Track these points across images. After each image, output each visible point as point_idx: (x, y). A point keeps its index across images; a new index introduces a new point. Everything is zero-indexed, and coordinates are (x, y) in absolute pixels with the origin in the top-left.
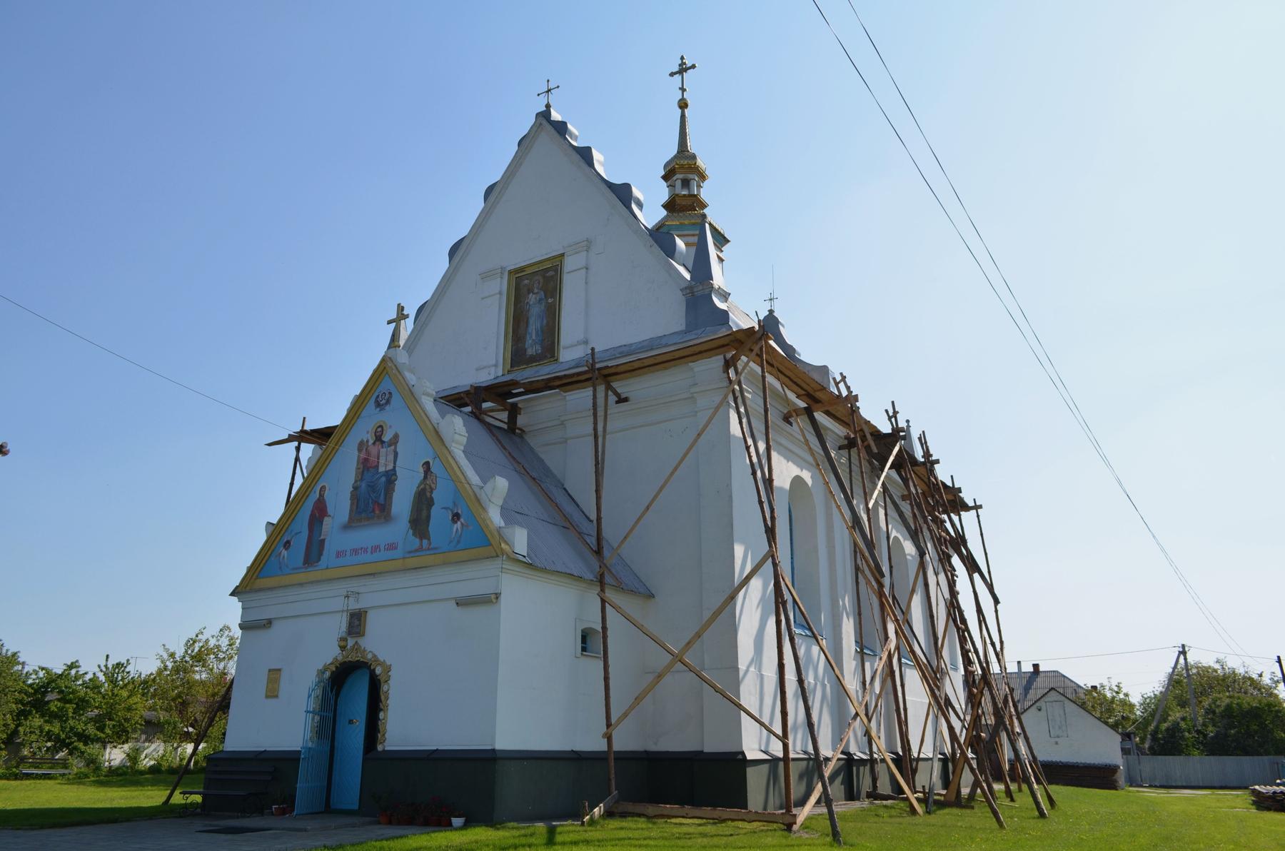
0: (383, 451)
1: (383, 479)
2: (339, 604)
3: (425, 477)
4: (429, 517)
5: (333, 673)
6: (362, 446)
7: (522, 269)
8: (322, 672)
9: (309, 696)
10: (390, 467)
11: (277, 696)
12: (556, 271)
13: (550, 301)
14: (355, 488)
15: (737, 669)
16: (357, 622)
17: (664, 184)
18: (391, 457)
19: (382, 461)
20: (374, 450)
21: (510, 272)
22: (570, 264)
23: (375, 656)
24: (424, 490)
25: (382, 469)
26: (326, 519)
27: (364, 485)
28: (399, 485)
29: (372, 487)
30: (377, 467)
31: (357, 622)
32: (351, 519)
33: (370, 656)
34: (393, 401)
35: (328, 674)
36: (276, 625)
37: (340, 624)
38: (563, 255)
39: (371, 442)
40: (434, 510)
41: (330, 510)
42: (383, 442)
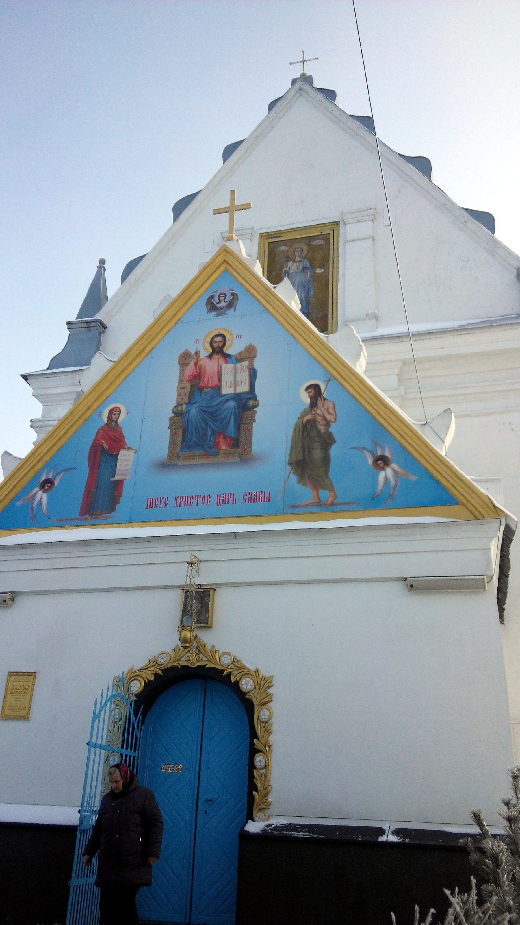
0: (228, 368)
1: (232, 404)
2: (180, 575)
3: (313, 405)
4: (326, 460)
5: (148, 684)
6: (185, 358)
7: (278, 234)
8: (122, 683)
9: (95, 717)
10: (244, 388)
11: (26, 718)
12: (327, 240)
13: (318, 271)
14: (178, 413)
15: (238, 879)
16: (198, 605)
17: (66, 333)
18: (244, 376)
19: (227, 378)
20: (210, 366)
21: (261, 235)
22: (348, 232)
23: (235, 661)
24: (313, 423)
25: (227, 390)
26: (123, 454)
27: (194, 410)
28: (261, 414)
29: (211, 414)
30: (218, 388)
31: (198, 605)
32: (172, 454)
33: (226, 660)
34: (240, 304)
35: (137, 687)
36: (20, 601)
37: (174, 602)
38: (337, 223)
39: (204, 354)
40: (334, 451)
41: (129, 440)
42: (226, 356)
